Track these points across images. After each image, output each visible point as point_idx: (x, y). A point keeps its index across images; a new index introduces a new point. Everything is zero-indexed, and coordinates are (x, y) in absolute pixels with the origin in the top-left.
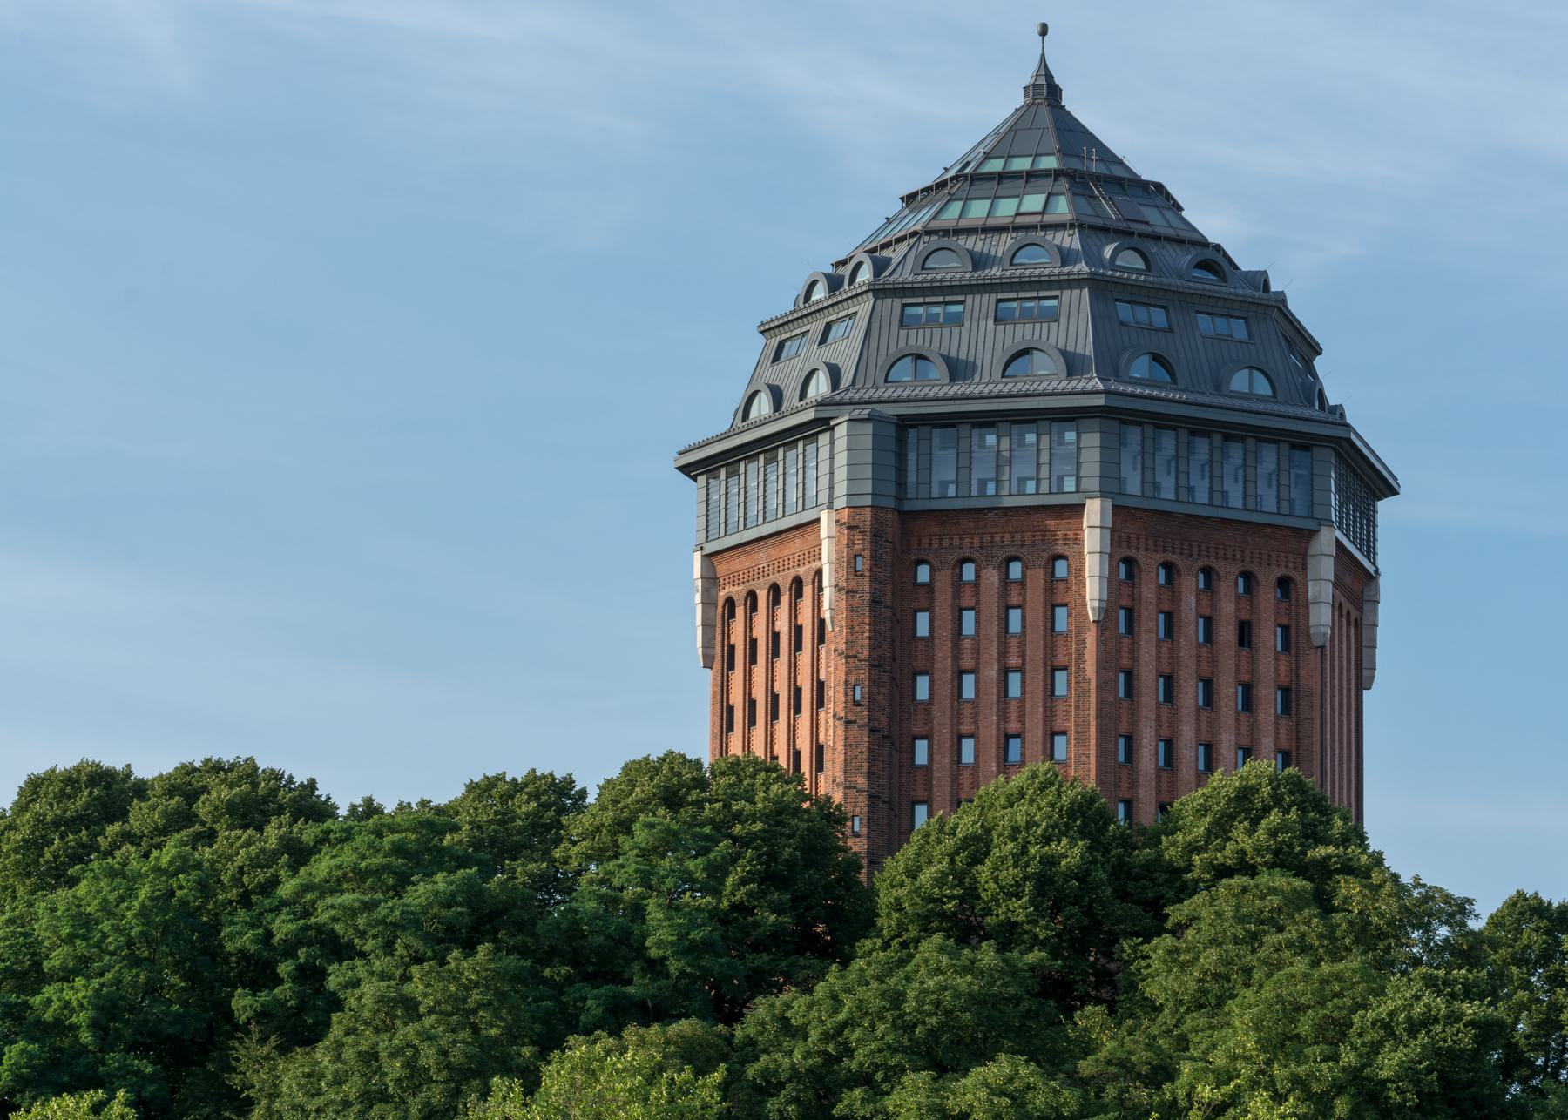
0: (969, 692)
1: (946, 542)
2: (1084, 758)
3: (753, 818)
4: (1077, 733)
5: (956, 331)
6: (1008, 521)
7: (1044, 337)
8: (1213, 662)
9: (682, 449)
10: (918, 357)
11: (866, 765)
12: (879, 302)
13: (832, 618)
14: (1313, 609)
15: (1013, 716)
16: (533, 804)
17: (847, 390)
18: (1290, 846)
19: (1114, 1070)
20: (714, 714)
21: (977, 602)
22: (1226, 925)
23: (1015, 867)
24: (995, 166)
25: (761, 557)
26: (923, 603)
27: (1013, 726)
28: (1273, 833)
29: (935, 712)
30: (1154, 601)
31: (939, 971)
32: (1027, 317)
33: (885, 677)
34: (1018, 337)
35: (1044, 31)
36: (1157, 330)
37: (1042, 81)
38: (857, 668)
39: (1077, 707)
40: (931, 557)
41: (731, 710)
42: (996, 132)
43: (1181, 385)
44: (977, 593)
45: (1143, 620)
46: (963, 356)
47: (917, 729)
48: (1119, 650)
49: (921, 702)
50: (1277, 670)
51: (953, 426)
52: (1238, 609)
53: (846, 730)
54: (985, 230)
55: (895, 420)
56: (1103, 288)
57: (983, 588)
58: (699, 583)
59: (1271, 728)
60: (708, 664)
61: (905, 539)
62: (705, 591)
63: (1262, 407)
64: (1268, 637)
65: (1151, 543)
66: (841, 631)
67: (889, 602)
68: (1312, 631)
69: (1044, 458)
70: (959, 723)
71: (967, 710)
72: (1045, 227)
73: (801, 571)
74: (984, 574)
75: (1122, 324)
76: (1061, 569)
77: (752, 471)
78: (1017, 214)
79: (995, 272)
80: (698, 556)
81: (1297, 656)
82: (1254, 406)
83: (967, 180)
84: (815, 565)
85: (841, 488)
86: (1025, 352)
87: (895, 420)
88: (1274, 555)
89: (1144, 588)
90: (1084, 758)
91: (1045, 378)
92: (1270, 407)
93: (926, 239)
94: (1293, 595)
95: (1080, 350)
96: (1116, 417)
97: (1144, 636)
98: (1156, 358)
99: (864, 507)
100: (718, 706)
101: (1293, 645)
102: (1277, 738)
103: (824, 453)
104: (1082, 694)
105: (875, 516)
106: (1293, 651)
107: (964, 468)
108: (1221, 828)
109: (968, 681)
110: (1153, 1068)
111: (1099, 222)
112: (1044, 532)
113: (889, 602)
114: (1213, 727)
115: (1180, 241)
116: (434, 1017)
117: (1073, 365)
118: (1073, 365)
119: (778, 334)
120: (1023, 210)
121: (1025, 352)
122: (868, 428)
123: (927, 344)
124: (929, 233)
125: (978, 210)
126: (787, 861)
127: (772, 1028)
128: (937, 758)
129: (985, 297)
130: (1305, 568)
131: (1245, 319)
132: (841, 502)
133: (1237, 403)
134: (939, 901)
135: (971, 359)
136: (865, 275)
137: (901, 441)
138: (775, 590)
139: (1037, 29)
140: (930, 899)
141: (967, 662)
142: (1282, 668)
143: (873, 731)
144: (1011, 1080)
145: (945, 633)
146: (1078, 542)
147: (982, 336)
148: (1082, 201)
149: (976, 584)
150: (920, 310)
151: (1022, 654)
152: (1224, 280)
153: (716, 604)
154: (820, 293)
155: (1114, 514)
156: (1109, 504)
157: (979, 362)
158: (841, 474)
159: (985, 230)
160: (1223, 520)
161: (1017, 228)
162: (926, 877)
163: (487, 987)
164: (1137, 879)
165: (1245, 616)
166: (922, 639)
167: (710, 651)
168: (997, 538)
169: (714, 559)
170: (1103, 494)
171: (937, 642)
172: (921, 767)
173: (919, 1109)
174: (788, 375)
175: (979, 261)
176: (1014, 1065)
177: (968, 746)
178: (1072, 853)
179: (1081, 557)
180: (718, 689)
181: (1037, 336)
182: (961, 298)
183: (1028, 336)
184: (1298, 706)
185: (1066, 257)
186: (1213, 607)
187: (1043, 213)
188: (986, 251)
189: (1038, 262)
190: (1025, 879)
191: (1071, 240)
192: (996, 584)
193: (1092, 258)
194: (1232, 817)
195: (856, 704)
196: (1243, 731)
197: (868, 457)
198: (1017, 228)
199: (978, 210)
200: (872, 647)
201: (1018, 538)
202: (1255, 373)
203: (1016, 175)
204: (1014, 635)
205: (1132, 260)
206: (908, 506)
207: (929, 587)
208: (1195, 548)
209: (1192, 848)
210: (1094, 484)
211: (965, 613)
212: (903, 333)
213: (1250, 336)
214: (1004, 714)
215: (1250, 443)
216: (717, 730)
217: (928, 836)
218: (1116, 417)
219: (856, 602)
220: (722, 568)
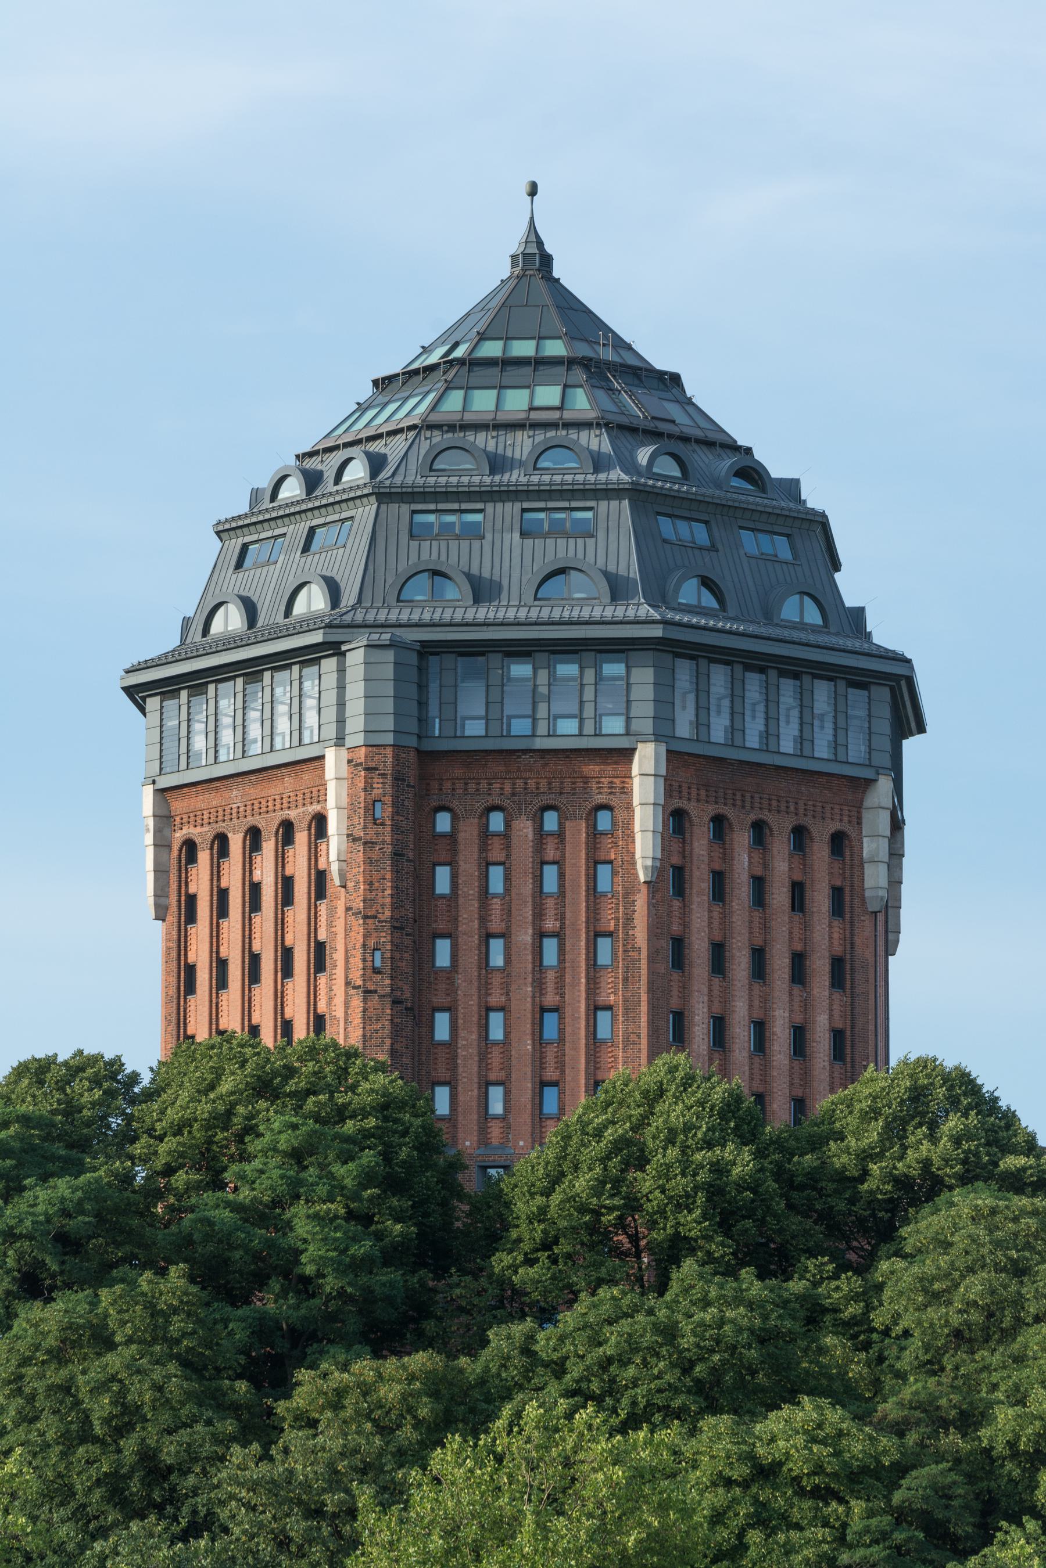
0: (497, 959)
1: (472, 786)
2: (633, 1037)
3: (364, 1113)
4: (626, 1009)
5: (476, 544)
6: (544, 766)
7: (580, 555)
8: (765, 927)
9: (128, 666)
10: (436, 573)
11: (388, 1041)
12: (384, 507)
13: (342, 875)
14: (868, 869)
15: (550, 987)
16: (97, 1094)
17: (354, 608)
18: (977, 1154)
19: (918, 1414)
20: (167, 973)
21: (508, 856)
22: (985, 1251)
23: (684, 1174)
24: (492, 349)
25: (235, 796)
26: (444, 856)
27: (550, 999)
28: (957, 1141)
29: (460, 980)
30: (706, 859)
31: (705, 1303)
32: (558, 531)
33: (408, 941)
34: (550, 556)
35: (533, 190)
36: (701, 549)
37: (533, 249)
38: (376, 930)
39: (626, 980)
40: (454, 804)
41: (191, 970)
42: (482, 306)
43: (731, 613)
44: (508, 847)
45: (695, 881)
46: (486, 574)
47: (438, 1000)
48: (670, 914)
49: (442, 969)
50: (831, 938)
51: (482, 654)
52: (791, 869)
53: (365, 1001)
54: (497, 426)
55: (418, 646)
56: (644, 499)
57: (515, 840)
58: (151, 823)
59: (826, 1003)
60: (161, 915)
61: (427, 782)
62: (158, 832)
63: (811, 638)
64: (820, 900)
65: (703, 793)
66: (356, 887)
67: (411, 855)
68: (867, 894)
69: (589, 694)
70: (488, 994)
71: (496, 979)
72: (567, 425)
73: (292, 814)
74: (516, 824)
75: (665, 541)
76: (604, 821)
77: (227, 698)
78: (532, 409)
79: (515, 477)
80: (148, 792)
81: (852, 923)
82: (802, 636)
83: (461, 369)
84: (316, 808)
85: (356, 723)
86: (562, 571)
87: (418, 646)
88: (828, 807)
89: (696, 844)
90: (633, 1037)
91: (584, 605)
92: (820, 639)
93: (428, 434)
94: (847, 853)
95: (622, 571)
96: (671, 649)
97: (696, 899)
98: (707, 583)
99: (385, 746)
100: (175, 964)
101: (847, 910)
102: (831, 1016)
103: (330, 680)
104: (631, 965)
105: (396, 757)
106: (847, 917)
107: (494, 705)
108: (895, 1133)
109: (497, 947)
110: (962, 1413)
111: (624, 420)
112: (586, 779)
113: (411, 855)
114: (766, 1002)
115: (710, 444)
116: (134, 1347)
117: (618, 589)
118: (618, 589)
119: (242, 535)
120: (537, 403)
121: (562, 571)
122: (390, 655)
123: (443, 558)
124: (431, 427)
125: (484, 401)
126: (404, 1162)
127: (518, 1361)
128: (462, 1034)
129: (508, 506)
130: (859, 823)
131: (788, 536)
132: (354, 739)
133: (786, 634)
134: (597, 1213)
135: (496, 578)
136: (357, 472)
137: (422, 670)
138: (254, 836)
139: (524, 189)
140: (583, 1209)
141: (496, 925)
142: (836, 936)
143: (396, 1002)
144: (820, 1426)
145: (470, 891)
146: (626, 791)
147: (509, 553)
148: (601, 394)
149: (506, 836)
150: (431, 518)
151: (561, 917)
152: (763, 490)
153: (169, 847)
154: (292, 490)
155: (668, 760)
156: (663, 748)
157: (505, 583)
158: (356, 707)
159: (497, 426)
160: (778, 768)
161: (535, 426)
162: (582, 1183)
163: (189, 1314)
164: (802, 1187)
165: (797, 877)
166: (442, 897)
167: (162, 901)
168: (532, 784)
169: (168, 795)
170: (658, 737)
171: (461, 900)
172: (442, 1044)
173: (728, 1457)
174: (265, 583)
175: (497, 464)
176: (818, 1408)
177: (496, 1020)
178: (742, 1162)
179: (629, 808)
180: (174, 945)
181: (571, 554)
182: (479, 506)
183: (561, 554)
184: (853, 980)
185: (599, 463)
186: (765, 866)
187: (561, 408)
188: (500, 451)
189: (565, 469)
190: (696, 1189)
191: (599, 442)
192: (531, 836)
193: (630, 466)
194: (905, 1122)
195: (377, 971)
196: (796, 1007)
197: (389, 689)
198: (535, 426)
199: (484, 401)
200: (395, 907)
201: (556, 784)
202: (806, 599)
203: (521, 362)
204: (550, 895)
205: (669, 467)
206: (428, 746)
207: (452, 837)
208: (748, 799)
209: (866, 1156)
210: (646, 726)
211: (492, 869)
212: (414, 544)
213: (795, 556)
214: (539, 985)
215: (773, 674)
216: (173, 992)
217: (570, 1137)
218: (671, 649)
219: (375, 854)
220: (179, 805)
